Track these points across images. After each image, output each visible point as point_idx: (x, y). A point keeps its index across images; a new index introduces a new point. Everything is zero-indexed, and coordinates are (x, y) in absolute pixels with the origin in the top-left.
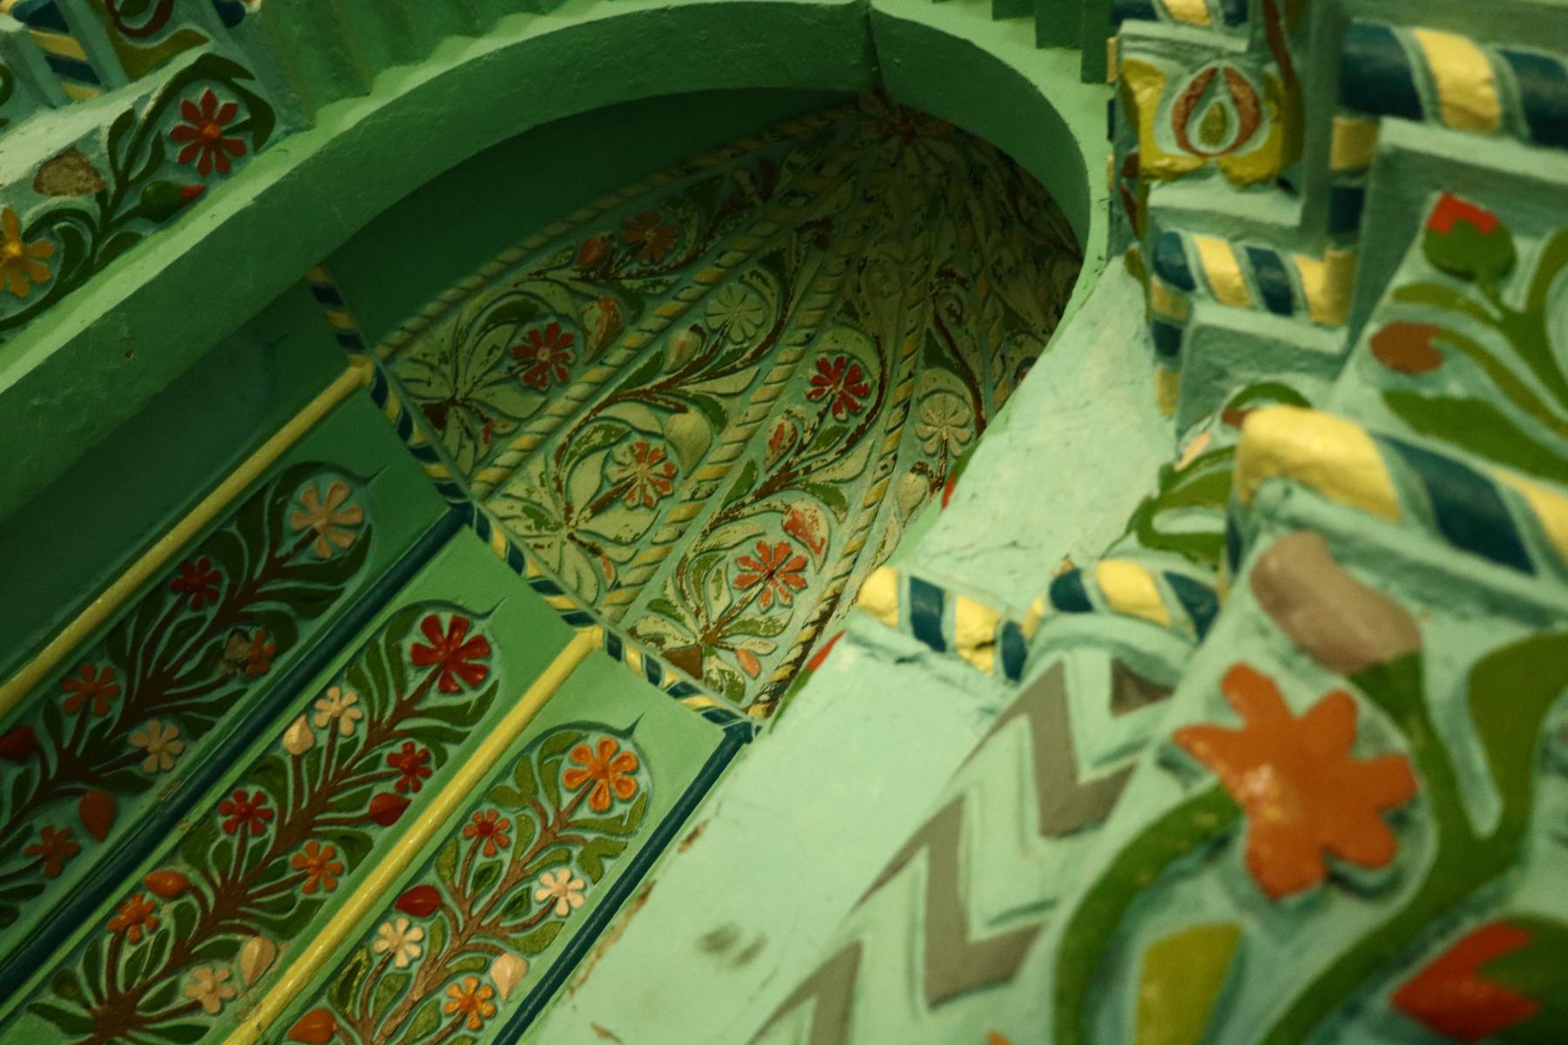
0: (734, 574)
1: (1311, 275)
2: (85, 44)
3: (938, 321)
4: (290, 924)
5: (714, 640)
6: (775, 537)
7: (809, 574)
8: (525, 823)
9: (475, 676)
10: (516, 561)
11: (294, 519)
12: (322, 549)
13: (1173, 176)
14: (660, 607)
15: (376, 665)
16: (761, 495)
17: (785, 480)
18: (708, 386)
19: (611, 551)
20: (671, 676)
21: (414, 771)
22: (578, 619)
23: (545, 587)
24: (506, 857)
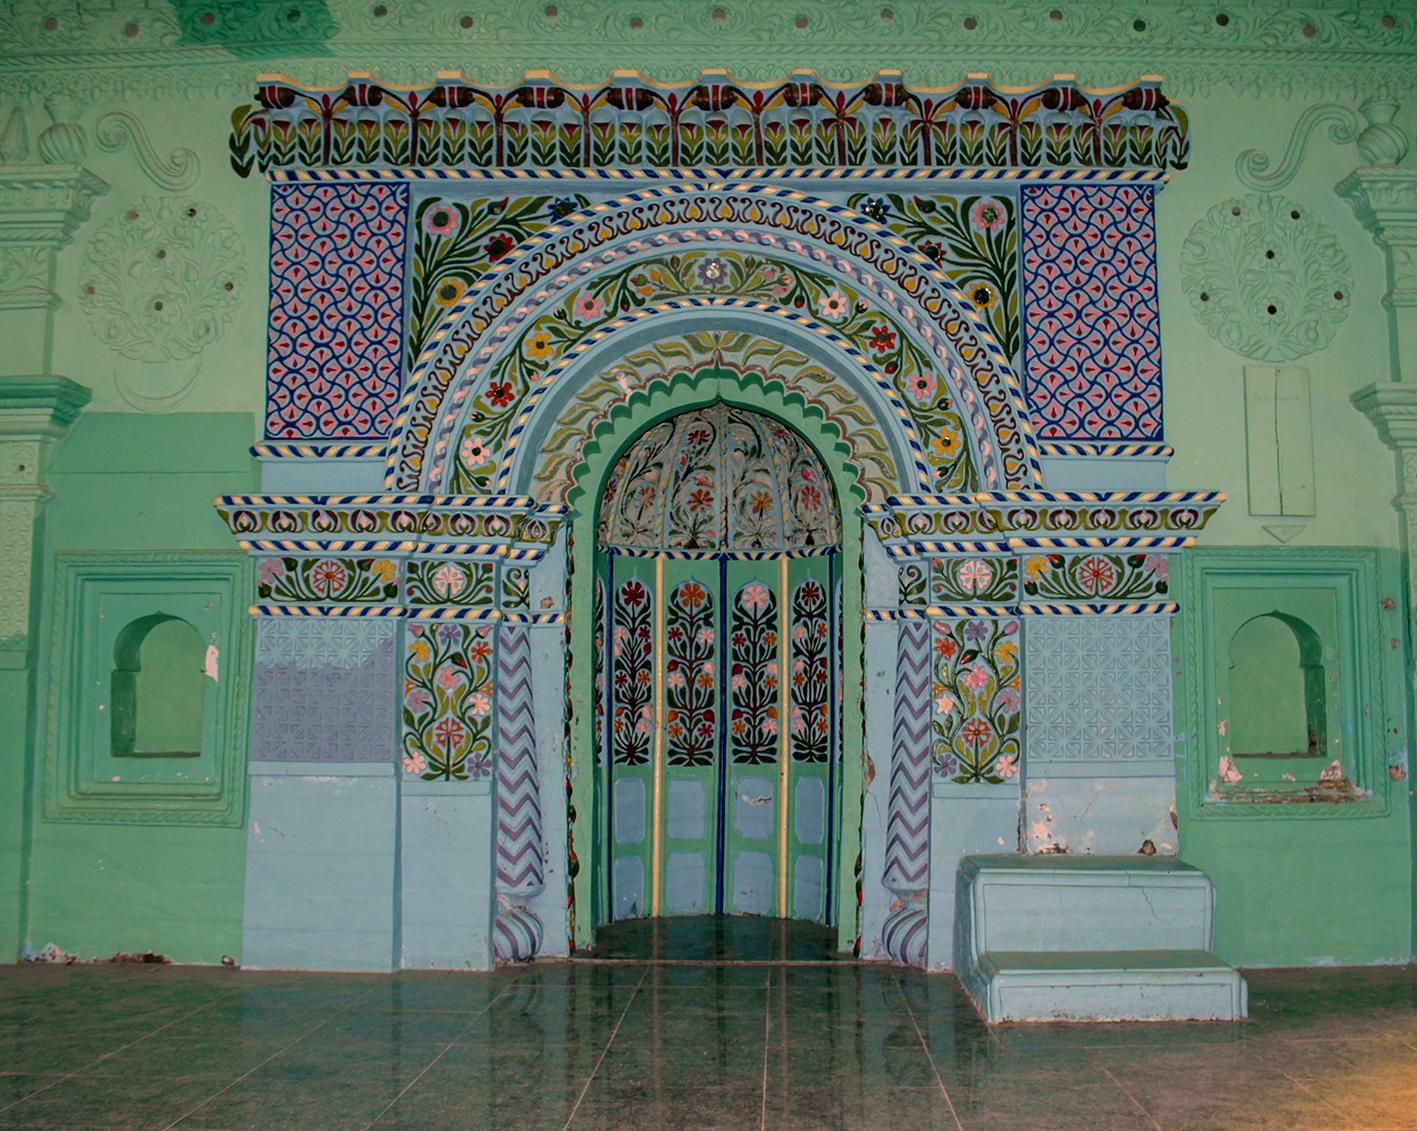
5: (695, 533)
6: (695, 489)
7: (712, 495)
8: (683, 625)
10: (631, 553)
11: (748, 606)
14: (673, 532)
17: (690, 470)
20: (693, 554)
21: (645, 634)
22: (657, 554)
24: (684, 637)
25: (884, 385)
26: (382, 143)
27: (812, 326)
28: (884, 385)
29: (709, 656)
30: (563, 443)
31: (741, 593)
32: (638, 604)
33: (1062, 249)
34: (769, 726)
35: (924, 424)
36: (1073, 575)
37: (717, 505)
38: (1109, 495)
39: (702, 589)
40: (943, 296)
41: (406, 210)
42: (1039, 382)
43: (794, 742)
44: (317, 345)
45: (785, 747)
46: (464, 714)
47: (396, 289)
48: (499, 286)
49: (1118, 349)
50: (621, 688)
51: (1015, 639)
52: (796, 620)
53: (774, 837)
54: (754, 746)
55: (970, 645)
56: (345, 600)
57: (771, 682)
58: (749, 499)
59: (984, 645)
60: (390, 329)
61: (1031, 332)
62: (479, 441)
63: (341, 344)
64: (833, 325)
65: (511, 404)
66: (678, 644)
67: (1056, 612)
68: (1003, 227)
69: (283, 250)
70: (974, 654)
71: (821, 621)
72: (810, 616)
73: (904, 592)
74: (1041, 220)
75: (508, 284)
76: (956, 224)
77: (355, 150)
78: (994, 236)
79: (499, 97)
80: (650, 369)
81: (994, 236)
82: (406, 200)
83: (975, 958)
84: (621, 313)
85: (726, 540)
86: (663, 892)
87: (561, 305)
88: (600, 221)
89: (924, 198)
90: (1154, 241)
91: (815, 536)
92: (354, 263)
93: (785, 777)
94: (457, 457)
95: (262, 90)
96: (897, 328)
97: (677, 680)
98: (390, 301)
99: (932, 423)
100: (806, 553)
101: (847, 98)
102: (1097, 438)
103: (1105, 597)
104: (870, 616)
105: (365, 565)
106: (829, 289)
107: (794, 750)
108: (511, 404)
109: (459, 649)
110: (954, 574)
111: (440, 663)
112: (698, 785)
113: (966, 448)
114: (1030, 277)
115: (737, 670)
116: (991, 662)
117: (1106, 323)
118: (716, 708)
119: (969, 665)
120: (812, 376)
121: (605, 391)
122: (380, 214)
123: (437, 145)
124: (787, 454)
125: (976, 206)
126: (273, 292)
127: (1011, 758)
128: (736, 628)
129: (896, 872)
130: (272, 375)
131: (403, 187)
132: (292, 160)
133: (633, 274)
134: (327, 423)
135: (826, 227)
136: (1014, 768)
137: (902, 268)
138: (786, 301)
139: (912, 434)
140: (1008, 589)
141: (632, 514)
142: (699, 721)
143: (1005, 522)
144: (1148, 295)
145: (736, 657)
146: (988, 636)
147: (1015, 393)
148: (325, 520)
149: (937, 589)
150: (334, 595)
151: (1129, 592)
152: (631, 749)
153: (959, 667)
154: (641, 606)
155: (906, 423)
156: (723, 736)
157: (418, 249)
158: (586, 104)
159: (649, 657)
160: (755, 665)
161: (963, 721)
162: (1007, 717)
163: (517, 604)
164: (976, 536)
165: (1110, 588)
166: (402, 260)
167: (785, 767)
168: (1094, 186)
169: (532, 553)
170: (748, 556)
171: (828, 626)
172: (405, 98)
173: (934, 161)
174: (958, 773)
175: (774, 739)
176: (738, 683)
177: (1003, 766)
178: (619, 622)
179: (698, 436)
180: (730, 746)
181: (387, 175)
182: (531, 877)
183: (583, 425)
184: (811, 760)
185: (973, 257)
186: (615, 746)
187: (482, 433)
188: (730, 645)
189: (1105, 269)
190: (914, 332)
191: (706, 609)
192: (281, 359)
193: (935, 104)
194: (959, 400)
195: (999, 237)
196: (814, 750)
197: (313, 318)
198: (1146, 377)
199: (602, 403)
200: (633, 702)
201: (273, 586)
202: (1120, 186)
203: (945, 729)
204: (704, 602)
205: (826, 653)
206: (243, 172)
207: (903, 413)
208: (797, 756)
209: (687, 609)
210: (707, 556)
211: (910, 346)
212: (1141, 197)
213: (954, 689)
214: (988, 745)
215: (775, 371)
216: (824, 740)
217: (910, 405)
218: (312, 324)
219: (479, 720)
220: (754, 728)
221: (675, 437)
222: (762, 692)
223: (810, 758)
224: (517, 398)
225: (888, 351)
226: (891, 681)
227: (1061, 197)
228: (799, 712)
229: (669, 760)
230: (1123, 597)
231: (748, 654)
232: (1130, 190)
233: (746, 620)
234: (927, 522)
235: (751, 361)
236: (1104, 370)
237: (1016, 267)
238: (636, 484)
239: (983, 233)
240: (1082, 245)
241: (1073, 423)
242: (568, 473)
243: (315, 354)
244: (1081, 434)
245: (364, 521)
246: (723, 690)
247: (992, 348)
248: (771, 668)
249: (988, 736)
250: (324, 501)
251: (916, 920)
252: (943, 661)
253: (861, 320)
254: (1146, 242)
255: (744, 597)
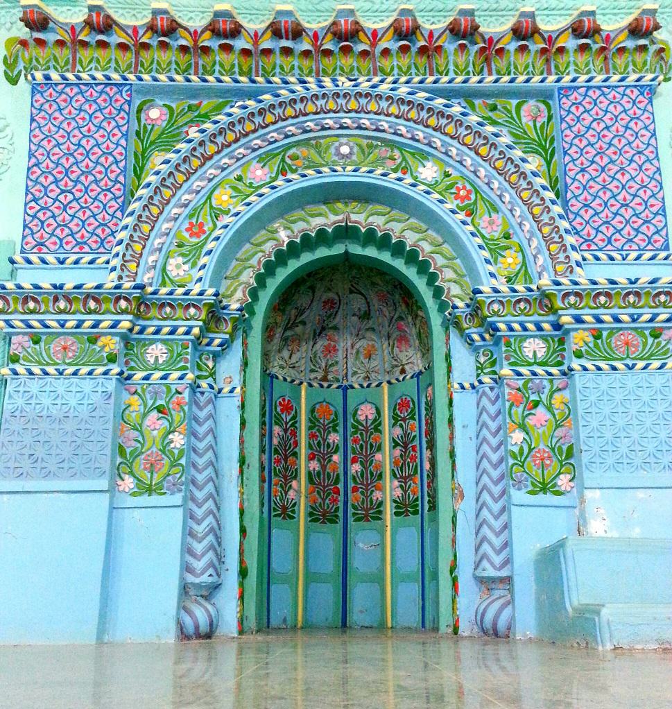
0: (322, 355)
1: (487, 336)
2: (167, 326)
3: (352, 285)
4: (296, 476)
5: (327, 372)
6: (326, 343)
7: (337, 347)
9: (291, 408)
10: (285, 380)
11: (362, 418)
12: (371, 417)
13: (467, 329)
14: (312, 371)
15: (278, 419)
16: (319, 335)
17: (323, 329)
18: (301, 318)
19: (297, 365)
20: (325, 384)
21: (294, 434)
22: (301, 383)
23: (293, 381)
24: (319, 439)
25: (464, 223)
26: (113, 60)
27: (414, 185)
28: (464, 223)
29: (335, 452)
30: (240, 273)
31: (357, 410)
32: (289, 414)
33: (589, 128)
34: (377, 495)
35: (495, 249)
36: (609, 344)
37: (340, 355)
38: (637, 280)
39: (332, 408)
40: (508, 156)
41: (129, 103)
42: (577, 214)
43: (395, 505)
44: (63, 192)
45: (389, 509)
46: (164, 448)
47: (121, 154)
48: (194, 149)
49: (632, 191)
50: (277, 462)
51: (566, 394)
52: (394, 447)
53: (383, 570)
54: (367, 510)
55: (534, 397)
56: (76, 365)
57: (380, 466)
58: (361, 350)
59: (544, 397)
60: (116, 181)
61: (569, 181)
62: (180, 260)
63: (80, 191)
64: (429, 186)
65: (203, 237)
66: (316, 442)
67: (599, 369)
68: (545, 119)
69: (40, 127)
70: (536, 404)
71: (412, 422)
72: (404, 420)
73: (480, 368)
74: (573, 109)
75: (201, 150)
76: (512, 118)
77: (93, 65)
78: (538, 125)
79: (196, 32)
80: (301, 225)
81: (538, 125)
82: (130, 96)
83: (570, 610)
84: (281, 177)
85: (346, 376)
86: (305, 609)
87: (238, 172)
88: (266, 108)
89: (490, 102)
90: (654, 121)
91: (407, 367)
92: (91, 136)
93: (389, 529)
94: (164, 270)
95: (25, 13)
96: (473, 186)
97: (315, 465)
98: (117, 162)
99: (500, 248)
100: (401, 379)
101: (436, 35)
102: (622, 250)
103: (633, 359)
104: (456, 386)
105: (93, 339)
106: (425, 163)
107: (394, 510)
108: (203, 237)
109: (163, 402)
110: (520, 348)
111: (149, 412)
112: (328, 539)
113: (524, 263)
114: (567, 146)
115: (354, 461)
116: (549, 408)
117: (623, 174)
118: (341, 486)
119: (533, 411)
120: (411, 229)
121: (270, 239)
122: (110, 104)
123: (152, 63)
124: (387, 314)
125: (525, 107)
126: (31, 155)
127: (569, 477)
128: (354, 433)
129: (485, 563)
130: (28, 211)
131: (128, 87)
132: (48, 68)
133: (290, 152)
134: (67, 243)
135: (424, 114)
136: (572, 484)
137: (477, 140)
138: (395, 171)
139: (486, 254)
140: (559, 359)
141: (286, 354)
142: (329, 494)
143: (559, 304)
144: (652, 156)
145: (354, 453)
146: (546, 391)
147: (561, 217)
148: (62, 304)
149: (507, 358)
150: (67, 361)
151: (652, 355)
152: (284, 508)
153: (526, 413)
154: (291, 416)
155: (480, 247)
156: (346, 503)
157: (138, 133)
158: (256, 37)
159: (296, 450)
160: (367, 456)
161: (530, 450)
162: (565, 448)
163: (206, 377)
164: (536, 318)
165: (637, 353)
166: (126, 136)
167: (388, 523)
168: (608, 87)
169: (217, 342)
170: (361, 386)
171: (417, 423)
172: (130, 32)
173: (494, 72)
174: (530, 488)
175: (381, 504)
176: (356, 468)
177: (563, 481)
178: (276, 424)
179: (330, 304)
180: (351, 511)
181: (116, 77)
182: (211, 571)
183: (254, 261)
184: (407, 515)
185: (525, 139)
186: (273, 505)
187: (183, 255)
188: (350, 445)
189: (620, 140)
190: (485, 188)
191: (333, 421)
192: (35, 200)
193: (495, 40)
194: (518, 230)
195: (542, 127)
196: (404, 508)
197: (60, 172)
198: (654, 209)
199: (269, 247)
200: (285, 477)
201: (21, 355)
202: (627, 87)
203: (520, 458)
204: (332, 417)
205: (416, 442)
206: (14, 81)
207: (479, 240)
208: (397, 514)
209: (322, 421)
210: (335, 385)
211: (482, 198)
212: (642, 94)
213: (523, 427)
214: (554, 465)
215: (386, 226)
216: (417, 500)
217: (483, 237)
218: (60, 176)
219: (176, 452)
220: (367, 497)
221: (314, 304)
222: (372, 474)
223: (406, 513)
224: (208, 233)
225: (466, 202)
226: (473, 429)
227: (586, 95)
228: (396, 483)
229: (309, 519)
230: (648, 358)
231: (362, 450)
232: (635, 90)
233: (360, 427)
234: (501, 307)
235: (371, 219)
236: (623, 205)
237: (555, 145)
238: (289, 333)
239: (531, 124)
240: (602, 125)
241: (603, 240)
242: (244, 292)
243: (61, 197)
244: (609, 247)
245: (92, 305)
246: (346, 473)
247: (544, 188)
248: (378, 456)
249: (552, 461)
250: (61, 287)
251: (502, 601)
252: (514, 408)
253: (448, 181)
254: (648, 122)
255: (359, 413)
